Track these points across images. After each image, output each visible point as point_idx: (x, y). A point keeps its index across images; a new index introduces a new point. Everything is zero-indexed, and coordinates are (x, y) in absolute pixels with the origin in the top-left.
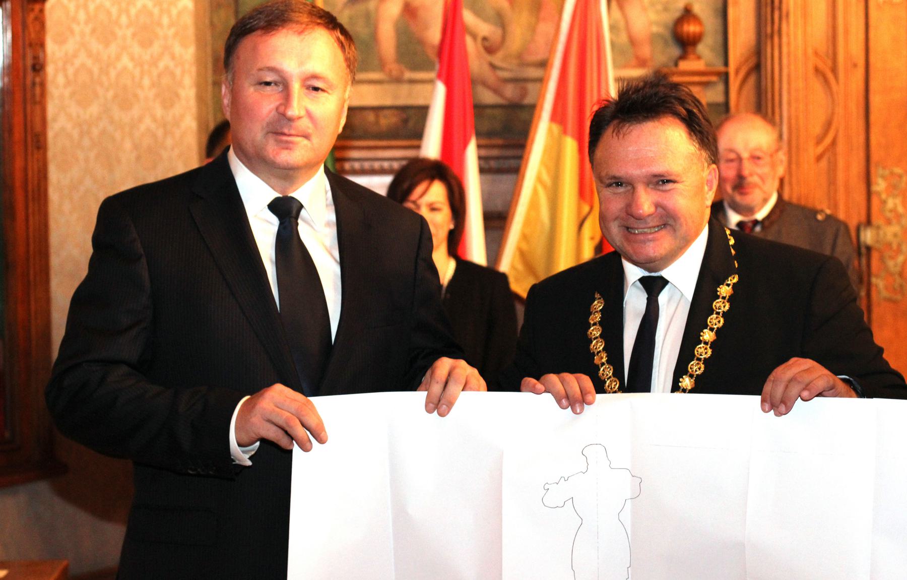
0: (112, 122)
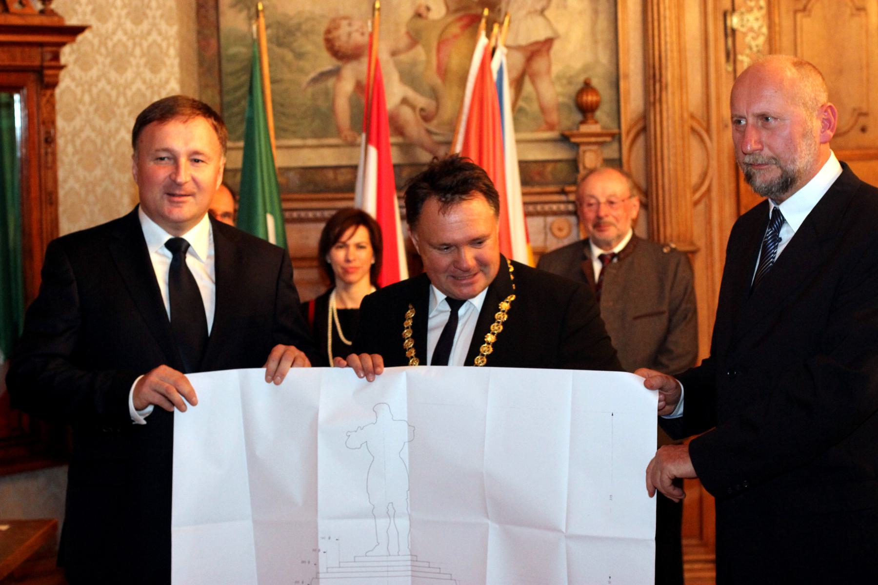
0: (113, 182)
